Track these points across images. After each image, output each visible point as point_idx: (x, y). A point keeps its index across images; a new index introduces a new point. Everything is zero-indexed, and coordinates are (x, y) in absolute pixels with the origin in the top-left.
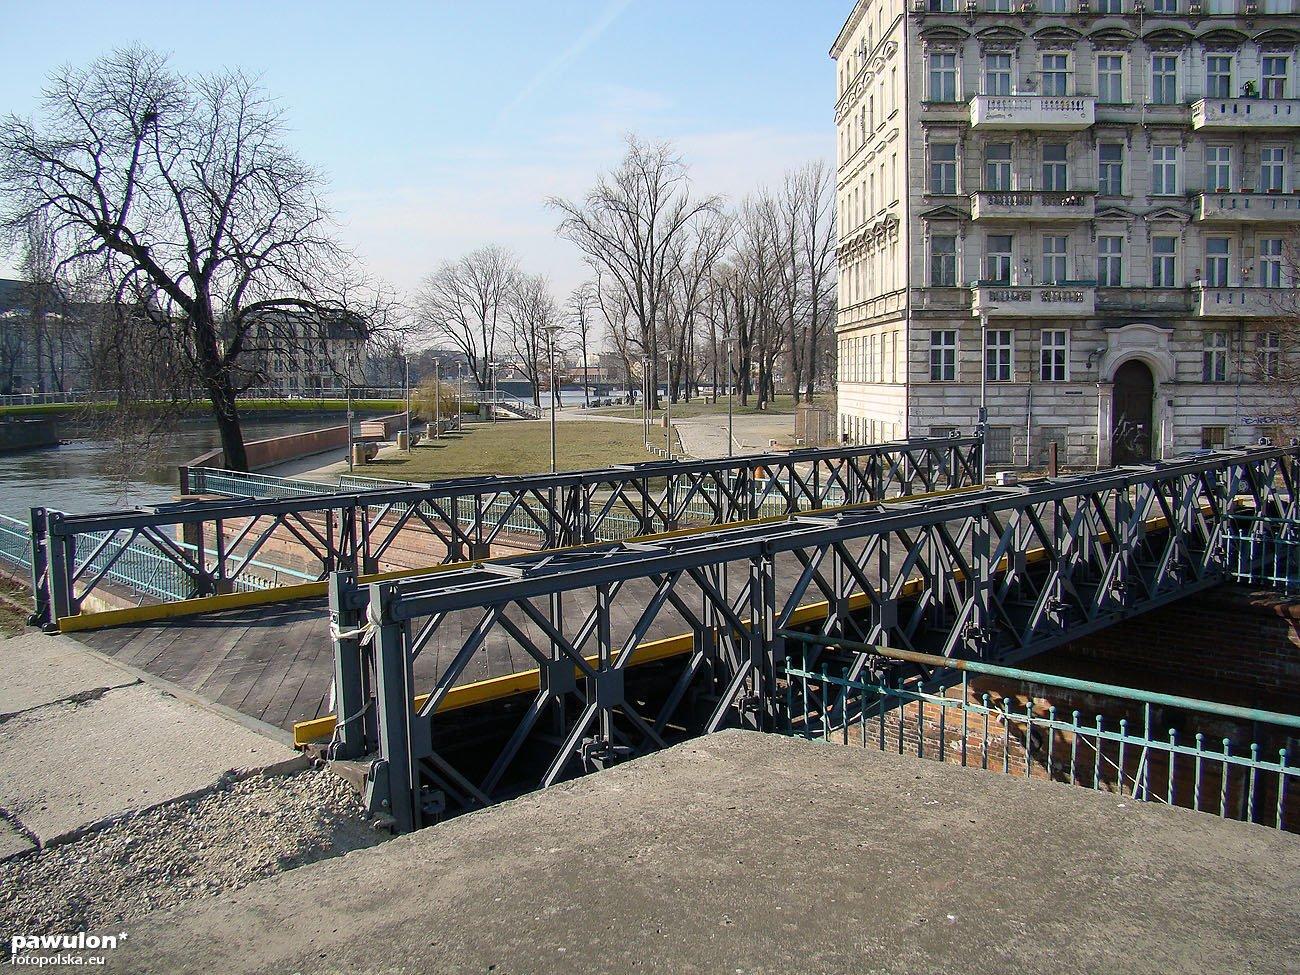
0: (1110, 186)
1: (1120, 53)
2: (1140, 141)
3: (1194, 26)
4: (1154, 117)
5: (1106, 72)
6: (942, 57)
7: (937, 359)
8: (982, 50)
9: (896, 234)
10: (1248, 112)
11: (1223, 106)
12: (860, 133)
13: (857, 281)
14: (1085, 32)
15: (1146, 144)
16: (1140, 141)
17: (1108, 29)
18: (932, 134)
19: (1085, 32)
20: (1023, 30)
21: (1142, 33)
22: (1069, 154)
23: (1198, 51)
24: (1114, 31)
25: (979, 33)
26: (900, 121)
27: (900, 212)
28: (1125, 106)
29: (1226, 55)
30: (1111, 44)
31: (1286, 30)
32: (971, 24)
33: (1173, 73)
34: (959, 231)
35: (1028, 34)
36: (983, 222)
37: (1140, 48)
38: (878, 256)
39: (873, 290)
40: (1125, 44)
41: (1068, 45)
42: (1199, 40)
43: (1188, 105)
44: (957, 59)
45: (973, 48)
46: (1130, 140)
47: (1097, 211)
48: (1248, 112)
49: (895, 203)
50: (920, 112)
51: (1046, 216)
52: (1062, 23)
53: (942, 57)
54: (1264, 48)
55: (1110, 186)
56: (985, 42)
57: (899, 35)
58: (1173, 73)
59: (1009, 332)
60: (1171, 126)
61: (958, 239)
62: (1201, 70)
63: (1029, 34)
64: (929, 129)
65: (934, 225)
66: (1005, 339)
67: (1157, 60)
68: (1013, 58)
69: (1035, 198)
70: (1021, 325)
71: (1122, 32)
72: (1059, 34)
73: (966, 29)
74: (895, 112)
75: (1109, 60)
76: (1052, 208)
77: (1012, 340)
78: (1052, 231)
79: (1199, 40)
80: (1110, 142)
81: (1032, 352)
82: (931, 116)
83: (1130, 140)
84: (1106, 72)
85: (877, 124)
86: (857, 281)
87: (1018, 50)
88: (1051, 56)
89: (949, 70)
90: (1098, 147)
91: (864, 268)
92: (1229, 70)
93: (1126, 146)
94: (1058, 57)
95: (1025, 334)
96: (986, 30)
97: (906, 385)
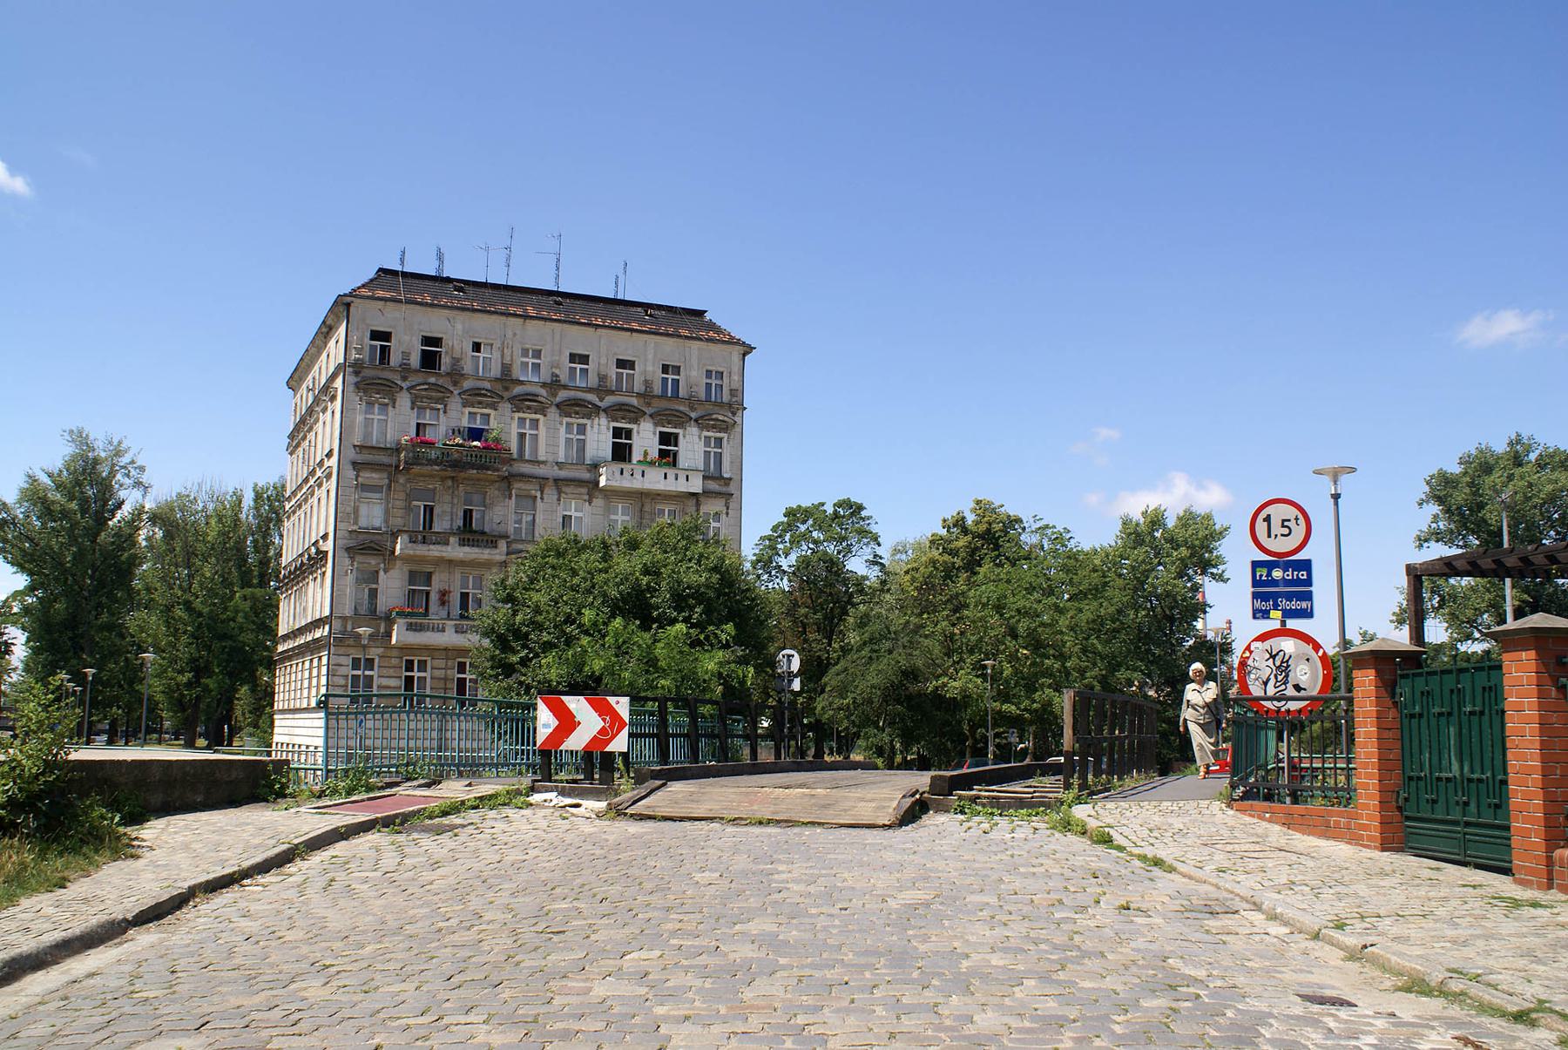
0: (524, 531)
1: (538, 416)
2: (550, 493)
3: (601, 400)
4: (563, 474)
5: (372, 416)
6: (428, 411)
7: (422, 685)
8: (413, 403)
9: (324, 566)
10: (643, 476)
11: (666, 474)
12: (306, 468)
13: (295, 608)
14: (506, 395)
15: (556, 497)
16: (550, 493)
17: (527, 394)
18: (361, 474)
19: (649, 411)
20: (451, 389)
21: (558, 399)
22: (437, 498)
23: (603, 420)
24: (531, 397)
25: (412, 387)
26: (333, 462)
27: (328, 546)
28: (540, 463)
29: (718, 435)
30: (529, 408)
31: (677, 411)
32: (404, 379)
33: (583, 437)
34: (382, 565)
35: (456, 392)
36: (405, 559)
37: (553, 413)
38: (311, 584)
39: (306, 617)
40: (542, 411)
41: (494, 407)
42: (605, 410)
43: (595, 466)
44: (390, 408)
45: (404, 400)
46: (542, 493)
47: (508, 554)
48: (643, 476)
49: (325, 537)
50: (351, 454)
51: (461, 555)
52: (488, 385)
53: (376, 405)
54: (702, 427)
55: (524, 531)
56: (416, 396)
57: (338, 383)
58: (583, 437)
59: (426, 661)
60: (579, 482)
61: (381, 573)
62: (700, 447)
63: (456, 392)
64: (358, 471)
65: (359, 558)
66: (423, 666)
67: (522, 420)
68: (441, 412)
69: (452, 539)
70: (436, 654)
71: (540, 399)
72: (485, 395)
73: (399, 383)
74: (331, 451)
75: (479, 416)
76: (467, 549)
77: (429, 668)
78: (467, 570)
79: (605, 410)
80: (525, 493)
81: (445, 679)
82: (360, 458)
83: (542, 493)
84: (372, 416)
85: (318, 460)
86: (295, 608)
87: (445, 406)
88: (475, 414)
89: (382, 417)
90: (514, 498)
91: (300, 595)
92: (537, 429)
93: (538, 498)
94: (482, 414)
95: (441, 663)
96: (419, 385)
97: (1000, 710)
